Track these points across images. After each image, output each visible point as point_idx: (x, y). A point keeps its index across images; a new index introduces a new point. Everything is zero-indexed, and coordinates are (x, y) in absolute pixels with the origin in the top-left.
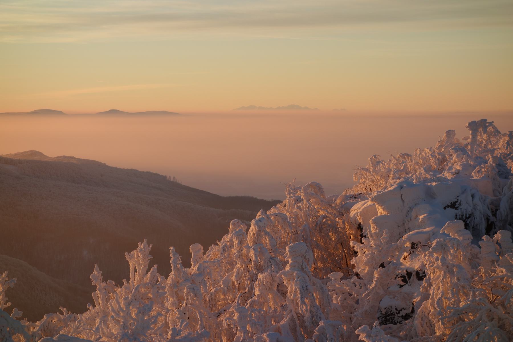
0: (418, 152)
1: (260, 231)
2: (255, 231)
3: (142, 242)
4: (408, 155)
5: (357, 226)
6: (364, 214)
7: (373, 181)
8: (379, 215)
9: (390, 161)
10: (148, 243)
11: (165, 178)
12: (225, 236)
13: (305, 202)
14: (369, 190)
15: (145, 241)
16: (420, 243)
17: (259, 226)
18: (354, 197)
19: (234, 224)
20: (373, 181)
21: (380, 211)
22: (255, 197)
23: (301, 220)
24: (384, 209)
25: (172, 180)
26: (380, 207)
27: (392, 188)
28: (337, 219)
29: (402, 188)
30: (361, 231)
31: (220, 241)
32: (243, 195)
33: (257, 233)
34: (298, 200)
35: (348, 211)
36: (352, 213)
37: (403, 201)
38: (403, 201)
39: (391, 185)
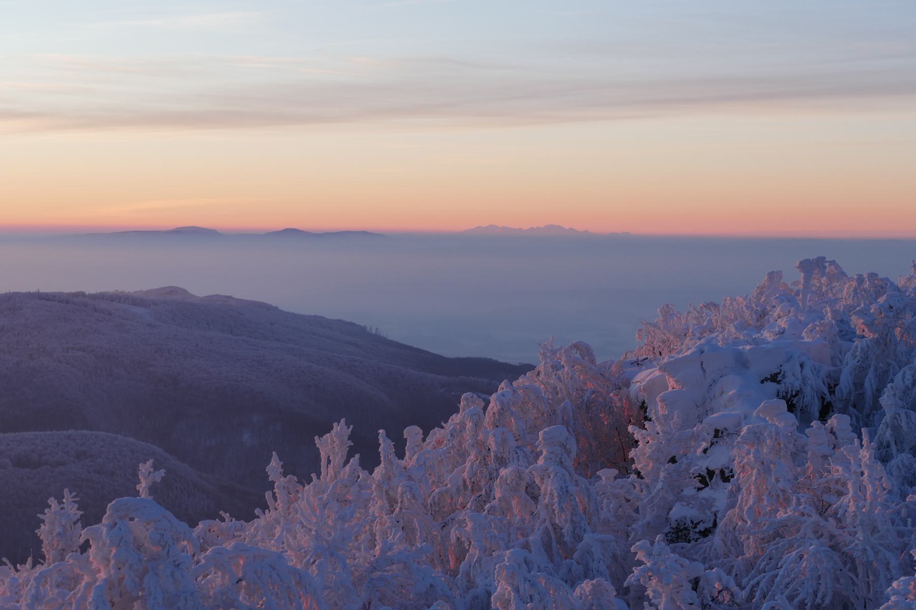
0: (728, 302)
1: (503, 409)
2: (495, 410)
3: (339, 422)
4: (716, 306)
5: (639, 404)
6: (652, 387)
7: (664, 342)
8: (670, 389)
9: (689, 313)
10: (348, 424)
11: (363, 329)
12: (454, 416)
13: (566, 369)
14: (658, 354)
15: (343, 420)
16: (726, 429)
17: (502, 403)
18: (637, 363)
19: (467, 399)
20: (664, 342)
21: (671, 383)
22: (494, 358)
23: (560, 396)
24: (676, 381)
25: (374, 332)
26: (671, 379)
27: (689, 353)
28: (612, 394)
29: (702, 352)
30: (645, 412)
31: (446, 422)
32: (477, 356)
33: (500, 414)
34: (557, 367)
35: (628, 384)
36: (635, 387)
37: (704, 371)
38: (704, 371)
39: (688, 348)
